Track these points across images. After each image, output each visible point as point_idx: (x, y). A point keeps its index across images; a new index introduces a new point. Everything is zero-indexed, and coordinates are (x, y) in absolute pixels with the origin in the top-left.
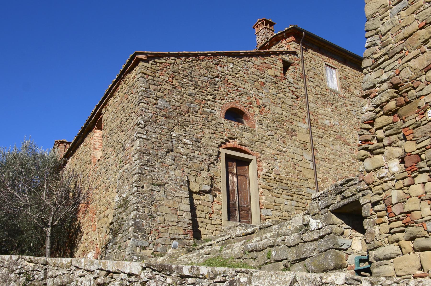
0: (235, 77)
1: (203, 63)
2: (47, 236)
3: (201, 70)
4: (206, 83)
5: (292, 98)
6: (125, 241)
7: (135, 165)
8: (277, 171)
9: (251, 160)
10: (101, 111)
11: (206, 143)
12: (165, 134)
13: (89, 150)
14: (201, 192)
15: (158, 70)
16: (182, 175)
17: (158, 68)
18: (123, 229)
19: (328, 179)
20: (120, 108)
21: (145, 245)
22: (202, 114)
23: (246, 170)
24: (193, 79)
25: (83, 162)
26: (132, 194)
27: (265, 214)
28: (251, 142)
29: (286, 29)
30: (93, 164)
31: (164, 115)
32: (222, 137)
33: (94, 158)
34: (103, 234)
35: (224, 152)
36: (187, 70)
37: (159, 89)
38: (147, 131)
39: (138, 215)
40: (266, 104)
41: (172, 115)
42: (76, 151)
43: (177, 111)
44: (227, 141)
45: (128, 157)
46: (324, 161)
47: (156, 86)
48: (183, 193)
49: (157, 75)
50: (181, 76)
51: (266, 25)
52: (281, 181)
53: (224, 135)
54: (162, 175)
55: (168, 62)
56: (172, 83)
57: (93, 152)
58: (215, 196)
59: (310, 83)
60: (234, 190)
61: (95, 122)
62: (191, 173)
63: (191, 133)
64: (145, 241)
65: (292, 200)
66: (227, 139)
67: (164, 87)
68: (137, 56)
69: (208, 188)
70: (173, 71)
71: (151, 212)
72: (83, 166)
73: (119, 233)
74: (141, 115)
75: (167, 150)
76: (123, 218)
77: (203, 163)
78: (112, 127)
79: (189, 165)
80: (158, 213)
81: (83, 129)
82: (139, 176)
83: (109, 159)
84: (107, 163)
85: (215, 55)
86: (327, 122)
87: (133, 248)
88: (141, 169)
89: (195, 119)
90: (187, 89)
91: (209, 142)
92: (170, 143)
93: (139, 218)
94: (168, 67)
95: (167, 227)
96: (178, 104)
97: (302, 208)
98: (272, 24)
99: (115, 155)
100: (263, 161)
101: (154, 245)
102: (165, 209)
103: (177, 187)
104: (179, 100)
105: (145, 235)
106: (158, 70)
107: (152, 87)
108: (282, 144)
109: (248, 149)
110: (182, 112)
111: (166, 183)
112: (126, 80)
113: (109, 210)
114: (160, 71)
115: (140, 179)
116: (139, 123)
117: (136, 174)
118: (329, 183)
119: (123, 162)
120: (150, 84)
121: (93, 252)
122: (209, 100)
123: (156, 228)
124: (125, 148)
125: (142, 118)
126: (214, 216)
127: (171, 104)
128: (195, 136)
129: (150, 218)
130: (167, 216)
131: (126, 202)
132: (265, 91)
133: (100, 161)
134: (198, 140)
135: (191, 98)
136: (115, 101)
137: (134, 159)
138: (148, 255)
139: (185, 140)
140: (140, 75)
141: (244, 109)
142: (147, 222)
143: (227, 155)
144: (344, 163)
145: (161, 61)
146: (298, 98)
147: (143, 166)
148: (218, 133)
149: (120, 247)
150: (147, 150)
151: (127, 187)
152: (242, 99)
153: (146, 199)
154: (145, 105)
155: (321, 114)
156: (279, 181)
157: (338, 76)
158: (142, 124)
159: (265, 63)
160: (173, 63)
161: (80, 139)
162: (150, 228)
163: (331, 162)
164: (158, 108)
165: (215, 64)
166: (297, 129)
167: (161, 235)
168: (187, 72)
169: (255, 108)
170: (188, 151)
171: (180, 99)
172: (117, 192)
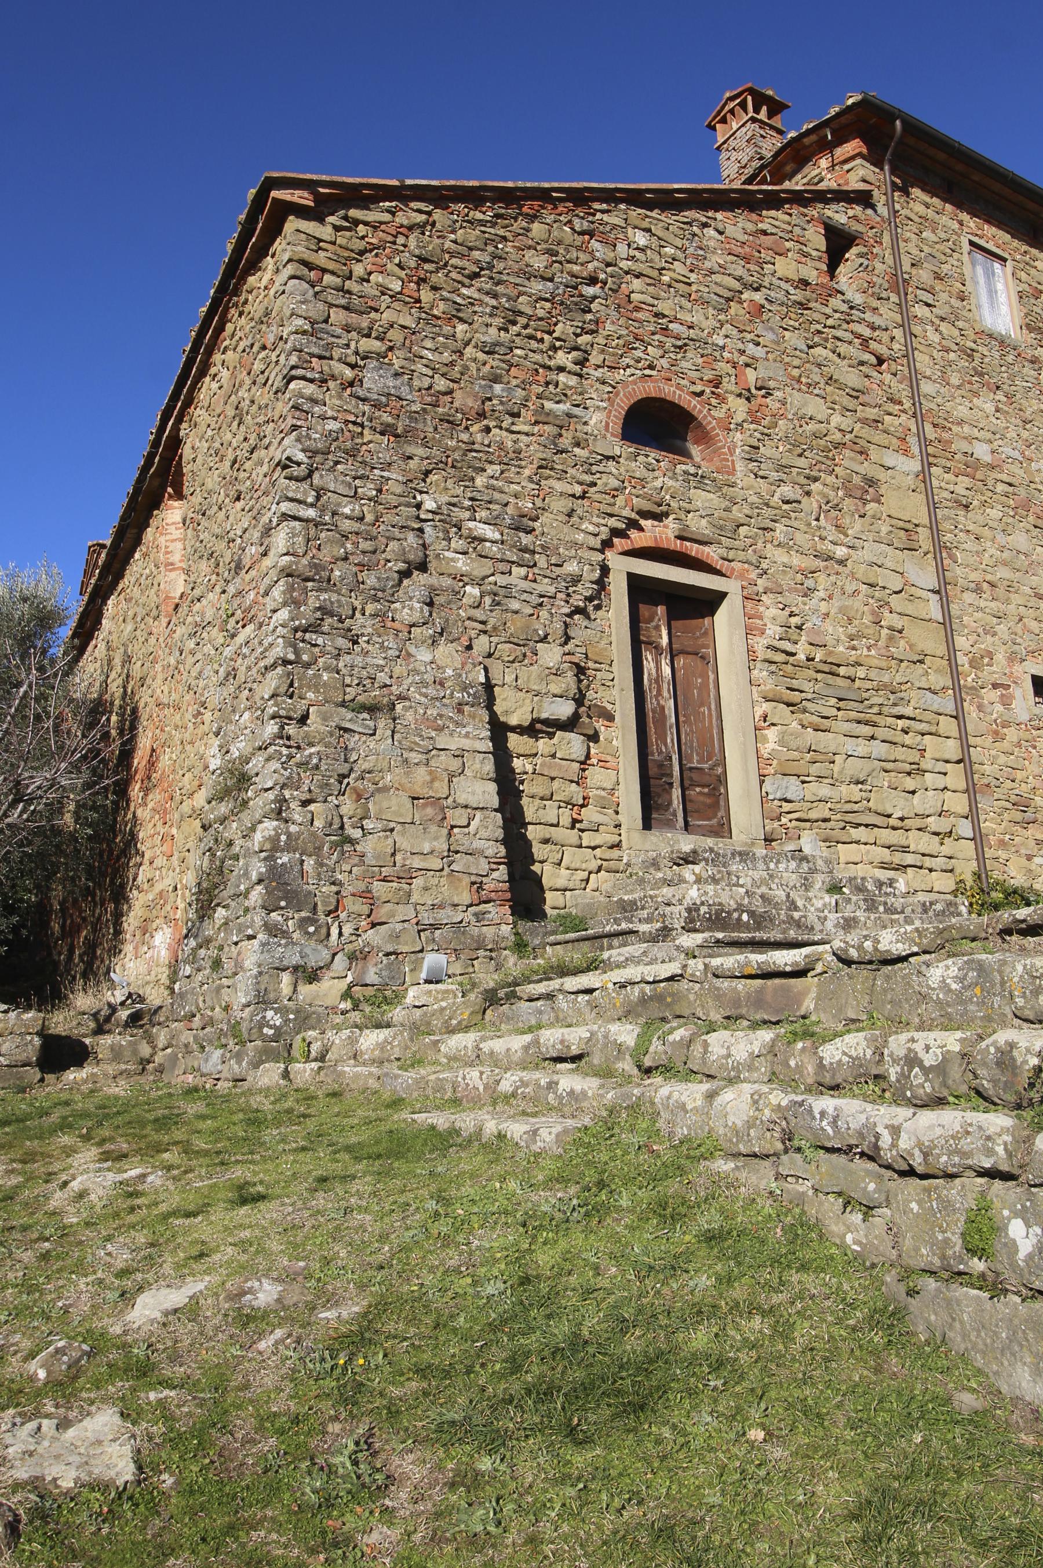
0: (656, 282)
1: (536, 226)
3: (529, 254)
4: (548, 305)
5: (862, 363)
6: (236, 944)
8: (818, 633)
9: (723, 595)
10: (176, 428)
11: (553, 532)
12: (394, 500)
14: (538, 726)
15: (362, 253)
16: (463, 664)
17: (360, 245)
19: (991, 655)
21: (312, 962)
22: (537, 423)
23: (706, 633)
24: (500, 289)
27: (778, 795)
28: (721, 528)
29: (833, 112)
31: (388, 425)
32: (615, 510)
35: (621, 566)
36: (476, 254)
39: (283, 838)
40: (772, 384)
41: (420, 426)
42: (122, 577)
43: (440, 410)
44: (633, 524)
46: (978, 590)
47: (356, 312)
48: (467, 735)
49: (359, 270)
50: (454, 275)
51: (757, 110)
53: (620, 501)
55: (401, 219)
56: (418, 301)
60: (663, 708)
61: (160, 478)
62: (497, 654)
63: (497, 496)
64: (313, 943)
65: (872, 737)
66: (634, 516)
67: (387, 316)
68: (274, 194)
69: (564, 710)
73: (218, 905)
74: (295, 428)
75: (401, 566)
76: (231, 844)
77: (544, 614)
79: (492, 622)
80: (368, 824)
81: (133, 499)
82: (289, 674)
83: (204, 601)
84: (198, 619)
85: (580, 198)
86: (982, 452)
89: (510, 444)
90: (475, 326)
91: (566, 529)
92: (411, 538)
93: (289, 848)
94: (401, 240)
95: (407, 876)
96: (441, 384)
97: (908, 767)
98: (776, 108)
100: (764, 598)
101: (352, 957)
103: (444, 711)
104: (445, 369)
106: (362, 253)
107: (337, 316)
108: (832, 534)
109: (711, 554)
110: (459, 416)
111: (401, 698)
112: (246, 302)
114: (369, 257)
115: (291, 685)
116: (288, 459)
117: (274, 666)
118: (994, 668)
120: (331, 305)
122: (561, 369)
123: (361, 886)
125: (298, 440)
126: (590, 814)
127: (416, 383)
128: (510, 510)
129: (334, 845)
130: (403, 833)
131: (244, 780)
134: (522, 524)
135: (493, 361)
138: (329, 1002)
139: (471, 524)
140: (290, 270)
142: (322, 865)
145: (371, 216)
146: (880, 361)
147: (305, 631)
148: (597, 497)
149: (217, 964)
150: (317, 567)
151: (247, 715)
152: (684, 364)
153: (317, 767)
154: (310, 389)
155: (961, 422)
156: (826, 668)
158: (299, 464)
159: (765, 233)
160: (422, 226)
161: (131, 533)
162: (334, 888)
163: (1000, 592)
164: (364, 400)
165: (582, 233)
166: (882, 475)
168: (477, 262)
169: (731, 398)
171: (452, 364)
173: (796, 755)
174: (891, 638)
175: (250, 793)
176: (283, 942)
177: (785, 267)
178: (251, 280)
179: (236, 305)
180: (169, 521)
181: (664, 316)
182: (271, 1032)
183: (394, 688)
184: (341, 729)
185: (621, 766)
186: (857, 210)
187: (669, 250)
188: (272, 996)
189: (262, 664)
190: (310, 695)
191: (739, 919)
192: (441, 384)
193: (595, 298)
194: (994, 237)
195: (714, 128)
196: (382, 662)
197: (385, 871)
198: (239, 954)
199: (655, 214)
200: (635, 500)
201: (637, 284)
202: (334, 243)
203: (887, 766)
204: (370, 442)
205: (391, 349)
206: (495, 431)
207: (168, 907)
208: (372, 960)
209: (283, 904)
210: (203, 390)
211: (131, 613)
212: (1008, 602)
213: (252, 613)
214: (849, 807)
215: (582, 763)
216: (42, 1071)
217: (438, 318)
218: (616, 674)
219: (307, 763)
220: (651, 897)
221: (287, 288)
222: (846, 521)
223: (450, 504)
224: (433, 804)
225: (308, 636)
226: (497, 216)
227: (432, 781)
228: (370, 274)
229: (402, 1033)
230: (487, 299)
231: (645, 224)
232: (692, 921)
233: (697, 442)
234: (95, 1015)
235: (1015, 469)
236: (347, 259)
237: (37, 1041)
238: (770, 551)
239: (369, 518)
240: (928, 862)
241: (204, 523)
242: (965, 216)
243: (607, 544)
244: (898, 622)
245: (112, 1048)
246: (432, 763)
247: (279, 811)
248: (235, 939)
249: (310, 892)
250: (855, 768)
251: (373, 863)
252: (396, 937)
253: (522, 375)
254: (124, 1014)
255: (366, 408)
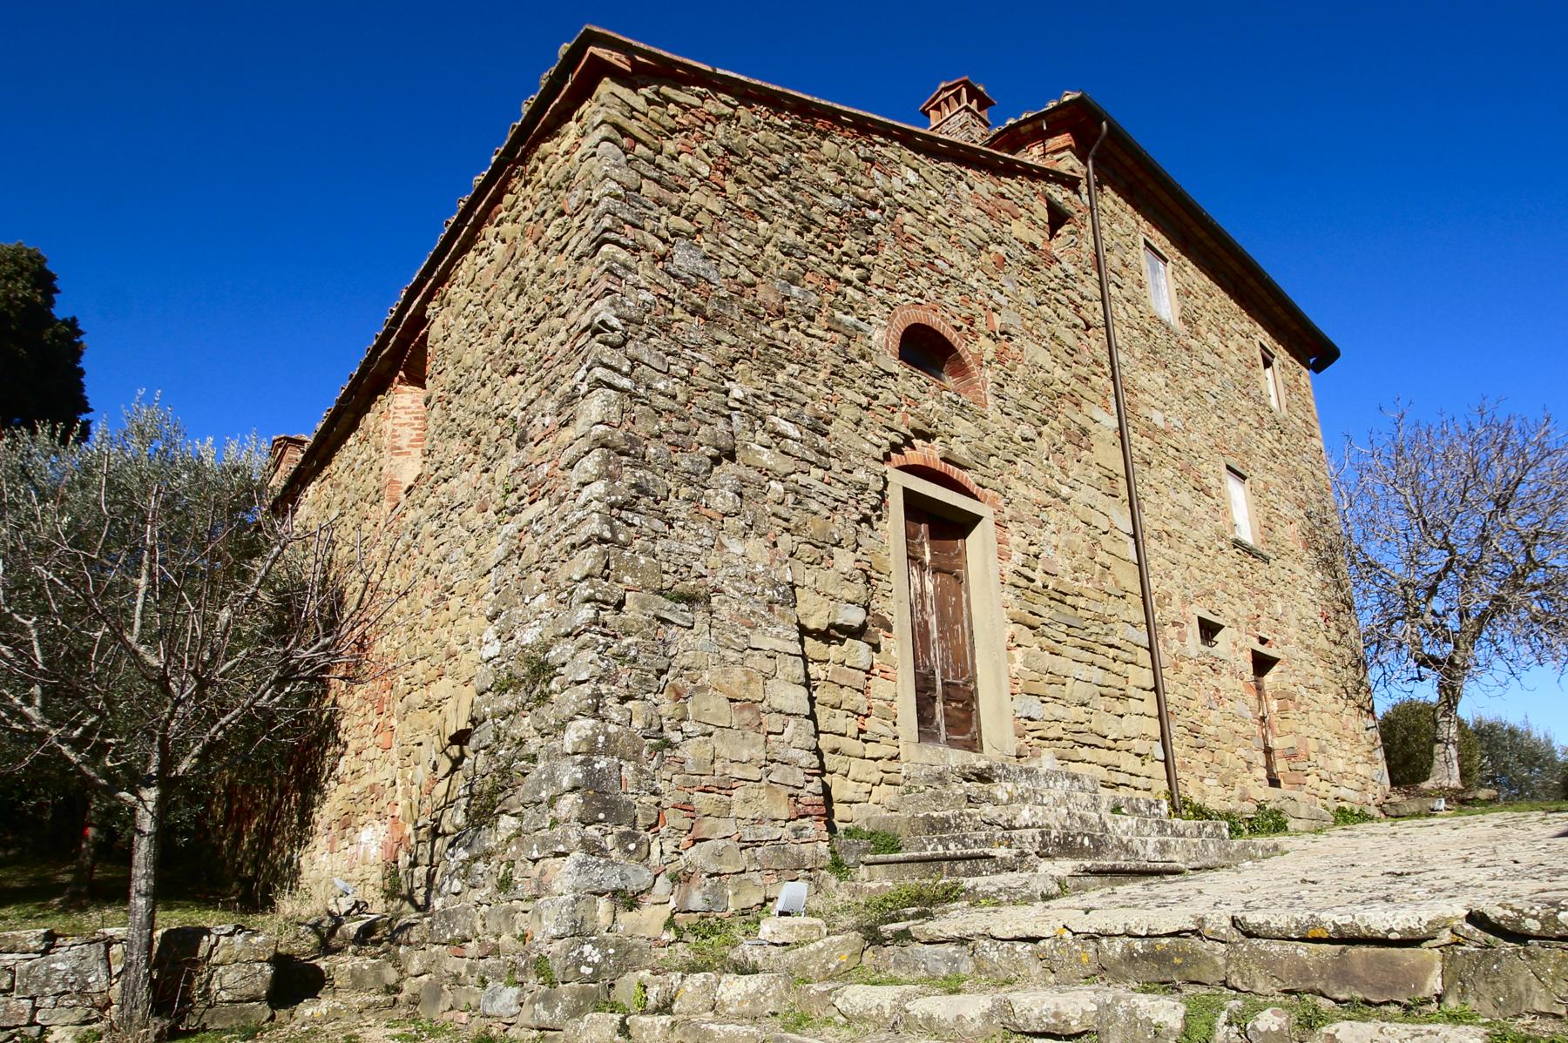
1: (826, 143)
2: (140, 832)
3: (821, 168)
4: (837, 220)
5: (1075, 326)
6: (535, 861)
7: (581, 500)
8: (1052, 563)
9: (978, 519)
10: (422, 307)
11: (845, 438)
12: (705, 384)
13: (375, 456)
14: (832, 631)
15: (673, 131)
16: (772, 561)
17: (670, 123)
18: (523, 794)
19: (1170, 596)
20: (505, 283)
21: (633, 887)
22: (829, 329)
23: (959, 555)
24: (797, 195)
25: (351, 497)
26: (568, 635)
29: (1051, 105)
30: (387, 505)
31: (698, 306)
32: (894, 425)
33: (392, 481)
34: (422, 773)
35: (900, 481)
36: (776, 157)
37: (675, 202)
38: (635, 362)
39: (601, 739)
40: (1012, 331)
41: (728, 313)
42: (330, 463)
43: (745, 300)
44: (908, 441)
45: (546, 468)
46: (1159, 538)
47: (667, 188)
48: (778, 636)
49: (670, 147)
50: (756, 172)
51: (970, 101)
52: (1060, 596)
53: (898, 417)
54: (696, 556)
56: (723, 190)
57: (387, 461)
58: (876, 648)
59: (1113, 290)
60: (926, 623)
61: (401, 356)
62: (798, 554)
63: (796, 395)
65: (1092, 664)
66: (909, 433)
67: (696, 198)
68: (591, 49)
70: (726, 147)
71: (656, 721)
72: (353, 511)
73: (504, 812)
74: (609, 292)
75: (712, 451)
76: (521, 742)
78: (469, 363)
79: (794, 520)
81: (356, 382)
82: (605, 553)
83: (454, 482)
84: (445, 501)
86: (1157, 418)
87: (582, 905)
88: (610, 523)
89: (806, 346)
90: (775, 225)
91: (855, 436)
92: (721, 424)
93: (608, 751)
94: (709, 127)
95: (726, 787)
96: (746, 276)
97: (1118, 693)
99: (477, 468)
100: (1009, 525)
101: (674, 879)
102: (714, 706)
103: (756, 609)
104: (748, 262)
105: (632, 836)
106: (673, 131)
107: (649, 188)
108: (1059, 475)
109: (968, 478)
110: (763, 310)
112: (535, 169)
113: (447, 681)
114: (680, 137)
115: (607, 566)
117: (587, 543)
119: (521, 492)
120: (643, 176)
121: (382, 829)
122: (848, 283)
123: (682, 796)
124: (530, 434)
125: (612, 305)
126: (873, 725)
127: (723, 269)
128: (807, 411)
129: (656, 749)
130: (722, 738)
131: (541, 670)
132: (1009, 288)
133: (415, 492)
134: (818, 427)
135: (791, 264)
136: (482, 260)
137: (575, 476)
138: (651, 934)
139: (775, 419)
140: (604, 130)
141: (953, 337)
142: (641, 772)
143: (908, 494)
144: (1201, 549)
145: (682, 97)
146: (1088, 327)
147: (621, 508)
148: (879, 410)
149: (505, 884)
150: (634, 442)
151: (543, 598)
152: (946, 298)
153: (635, 660)
154: (623, 255)
155: (1144, 391)
156: (1057, 596)
157: (1173, 286)
158: (613, 330)
159: (1002, 196)
160: (728, 119)
161: (346, 418)
162: (655, 799)
163: (1174, 541)
164: (675, 277)
165: (865, 160)
166: (1092, 428)
167: (703, 828)
168: (777, 165)
169: (982, 337)
170: (785, 465)
171: (755, 257)
172: (492, 619)
173: (1036, 676)
174: (1103, 574)
175: (554, 685)
176: (602, 861)
177: (1019, 229)
178: (546, 147)
179: (522, 174)
180: (399, 405)
181: (931, 251)
182: (590, 971)
183: (709, 579)
184: (659, 618)
185: (899, 678)
186: (1068, 193)
187: (932, 193)
188: (588, 927)
189: (568, 541)
190: (628, 579)
191: (1082, 844)
192: (746, 276)
193: (876, 221)
194: (1160, 241)
195: (927, 114)
196: (698, 550)
197: (706, 781)
198: (543, 873)
199: (921, 157)
200: (910, 418)
201: (909, 217)
202: (646, 115)
203: (1103, 690)
204: (681, 320)
205: (699, 231)
206: (793, 331)
207: (383, 803)
208: (695, 883)
209: (601, 816)
210: (465, 265)
211: (338, 499)
212: (1179, 550)
213: (547, 486)
214: (1077, 727)
215: (867, 672)
216: (273, 1008)
217: (742, 210)
218: (893, 586)
219: (625, 655)
220: (969, 815)
221: (598, 151)
222: (1068, 464)
223: (755, 396)
224: (750, 707)
225: (624, 514)
226: (794, 126)
227: (749, 682)
228: (680, 153)
229: (776, 981)
230: (785, 202)
231: (915, 164)
232: (1044, 845)
233: (953, 374)
234: (315, 927)
235: (1179, 436)
236: (659, 133)
237: (268, 970)
238: (1013, 482)
239: (681, 397)
240: (1135, 781)
241: (456, 401)
242: (1140, 218)
243: (887, 457)
244: (1108, 560)
245: (352, 973)
246: (747, 663)
247: (595, 709)
248: (535, 855)
249: (630, 804)
250: (1074, 690)
251: (694, 771)
252: (718, 855)
253: (817, 282)
254: (352, 927)
255: (677, 286)
